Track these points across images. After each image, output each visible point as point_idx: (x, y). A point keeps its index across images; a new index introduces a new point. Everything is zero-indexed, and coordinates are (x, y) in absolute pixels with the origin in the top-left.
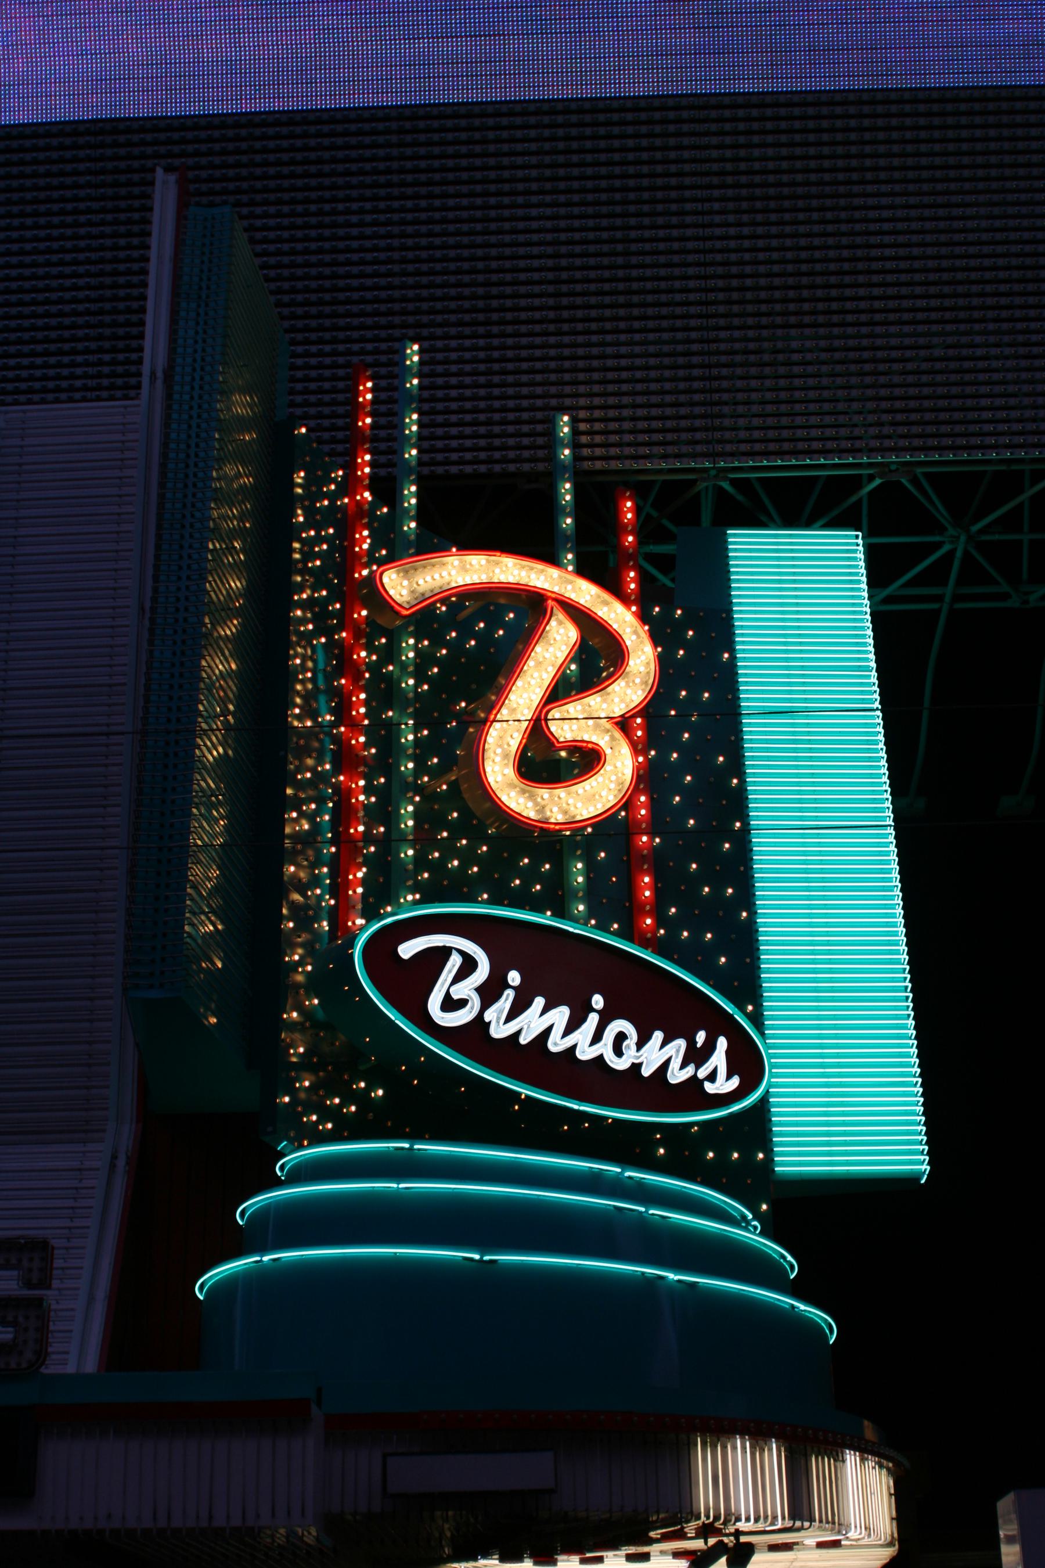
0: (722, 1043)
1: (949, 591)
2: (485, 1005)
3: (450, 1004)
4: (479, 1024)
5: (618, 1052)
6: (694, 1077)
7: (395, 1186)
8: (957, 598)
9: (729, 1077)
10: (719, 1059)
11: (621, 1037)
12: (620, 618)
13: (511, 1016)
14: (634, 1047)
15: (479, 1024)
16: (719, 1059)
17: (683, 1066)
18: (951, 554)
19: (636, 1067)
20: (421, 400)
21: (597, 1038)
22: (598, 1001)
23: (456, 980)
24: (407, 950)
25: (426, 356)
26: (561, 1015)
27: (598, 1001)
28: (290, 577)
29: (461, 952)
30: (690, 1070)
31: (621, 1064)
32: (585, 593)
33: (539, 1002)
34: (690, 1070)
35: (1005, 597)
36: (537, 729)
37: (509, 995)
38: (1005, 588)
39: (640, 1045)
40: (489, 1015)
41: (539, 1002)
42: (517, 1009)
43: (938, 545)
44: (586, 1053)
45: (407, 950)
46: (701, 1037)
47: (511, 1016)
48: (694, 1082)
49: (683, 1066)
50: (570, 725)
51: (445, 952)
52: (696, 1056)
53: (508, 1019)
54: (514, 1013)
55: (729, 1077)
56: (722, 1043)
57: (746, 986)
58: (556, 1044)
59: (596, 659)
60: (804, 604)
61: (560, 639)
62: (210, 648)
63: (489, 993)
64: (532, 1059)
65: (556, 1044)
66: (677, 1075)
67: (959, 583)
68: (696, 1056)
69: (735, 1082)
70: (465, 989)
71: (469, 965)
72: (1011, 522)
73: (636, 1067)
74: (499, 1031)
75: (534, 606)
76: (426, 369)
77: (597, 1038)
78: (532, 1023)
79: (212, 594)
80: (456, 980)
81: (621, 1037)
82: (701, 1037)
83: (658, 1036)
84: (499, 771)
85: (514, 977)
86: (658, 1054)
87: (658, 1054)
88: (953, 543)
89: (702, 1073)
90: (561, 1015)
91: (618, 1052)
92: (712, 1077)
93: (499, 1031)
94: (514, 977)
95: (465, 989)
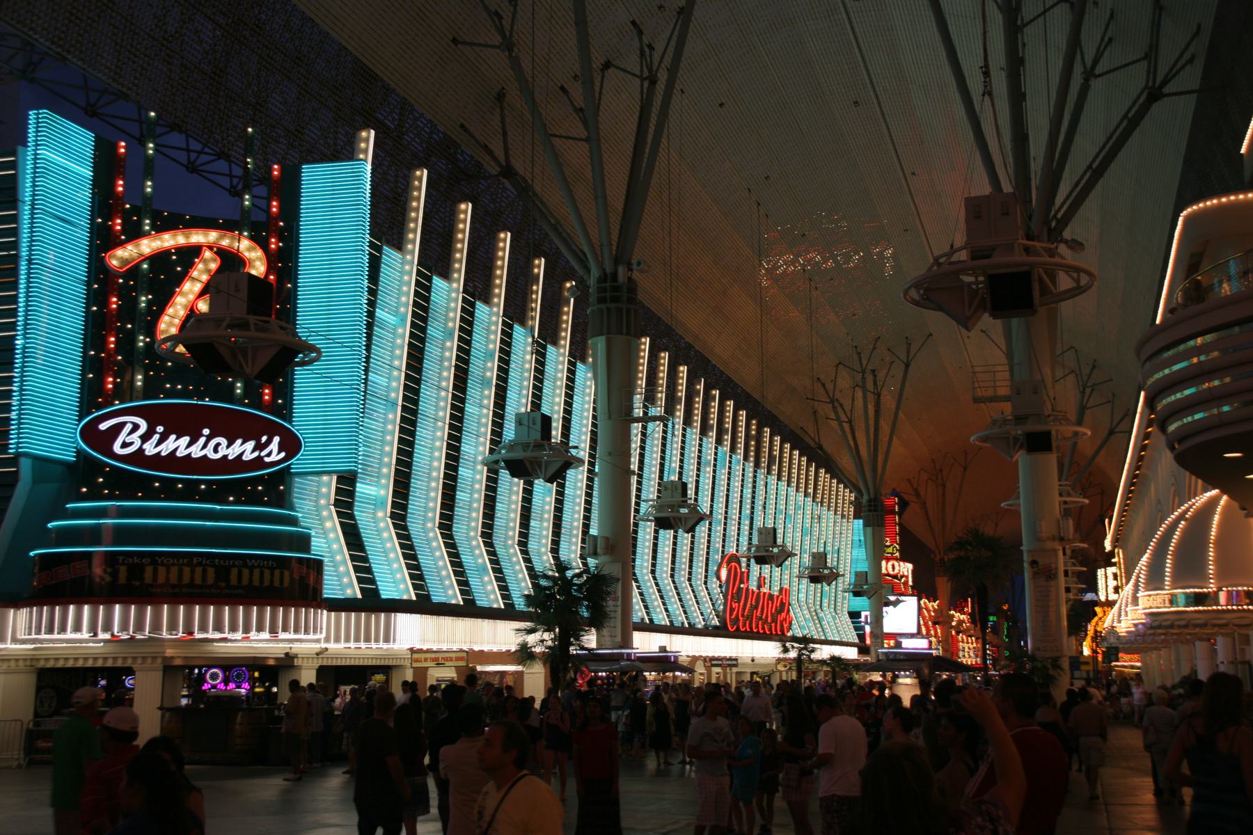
4: (141, 450)
7: (1185, 421)
9: (279, 452)
10: (274, 445)
11: (218, 444)
15: (141, 450)
16: (274, 445)
20: (1024, 683)
23: (130, 434)
24: (103, 426)
26: (185, 440)
30: (256, 454)
34: (256, 454)
37: (157, 437)
40: (145, 446)
45: (103, 426)
48: (260, 458)
51: (124, 424)
54: (159, 443)
55: (279, 452)
56: (277, 439)
63: (145, 438)
64: (170, 462)
66: (248, 457)
68: (259, 447)
69: (283, 455)
70: (135, 437)
71: (136, 427)
73: (225, 457)
79: (634, 479)
81: (218, 444)
82: (264, 439)
86: (244, 449)
87: (244, 449)
89: (263, 454)
90: (250, 445)
92: (269, 455)
95: (135, 437)
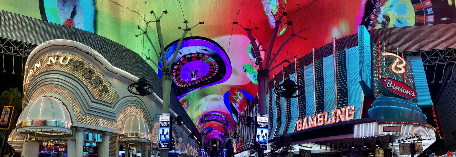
3: (389, 85)
10: (413, 93)
12: (402, 59)
16: (413, 93)
24: (385, 80)
26: (399, 88)
28: (450, 6)
32: (400, 57)
36: (396, 66)
45: (385, 80)
50: (399, 66)
52: (411, 93)
58: (399, 90)
62: (295, 101)
63: (393, 85)
65: (399, 90)
68: (411, 93)
72: (432, 56)
75: (396, 58)
78: (396, 88)
84: (387, 85)
88: (428, 58)
90: (399, 88)
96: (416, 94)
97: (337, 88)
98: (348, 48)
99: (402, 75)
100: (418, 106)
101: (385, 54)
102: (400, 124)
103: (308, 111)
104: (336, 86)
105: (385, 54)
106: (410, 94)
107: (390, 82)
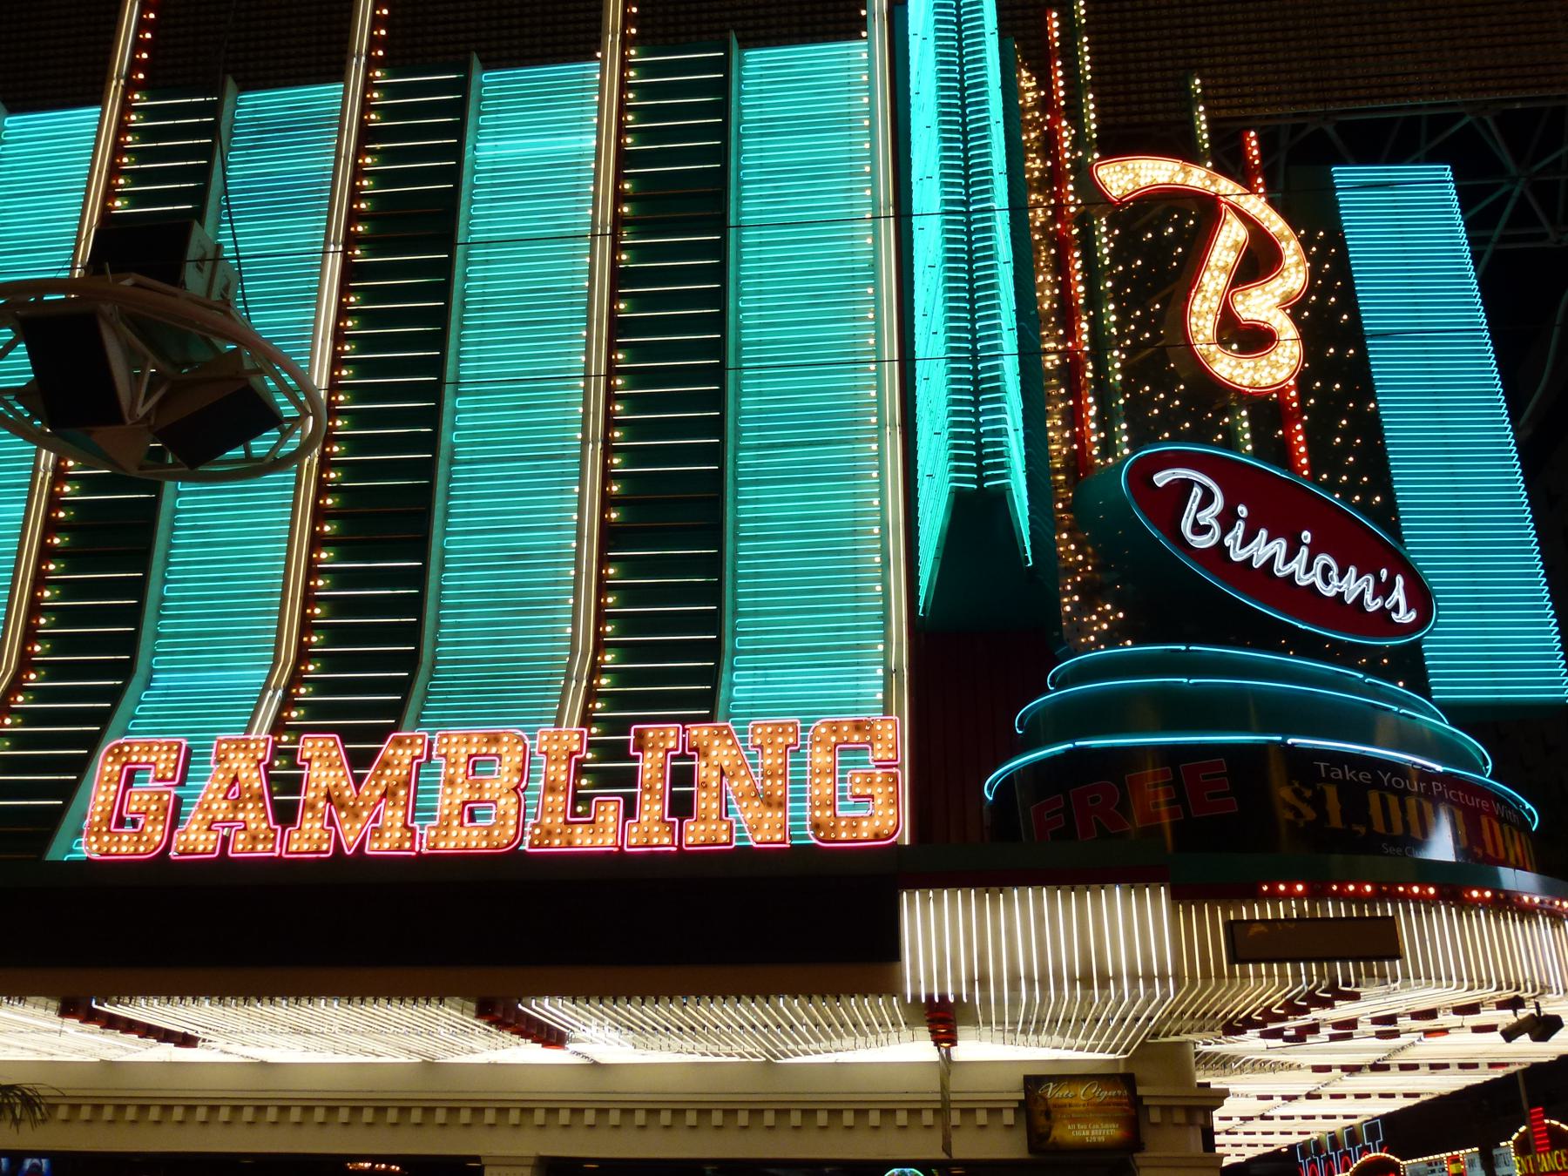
0: (1399, 580)
1: (1496, 234)
2: (1224, 533)
3: (1200, 529)
5: (1327, 582)
6: (1383, 607)
8: (1503, 239)
10: (1399, 594)
13: (1245, 544)
14: (1336, 578)
15: (1221, 549)
16: (1399, 594)
17: (1374, 598)
18: (1508, 195)
19: (1340, 595)
21: (1309, 569)
22: (1306, 536)
24: (1162, 479)
25: (1092, 18)
27: (1306, 536)
29: (1201, 485)
30: (1379, 601)
31: (1329, 592)
33: (1263, 533)
35: (1544, 236)
38: (1548, 228)
39: (1341, 576)
40: (1228, 541)
41: (1263, 533)
42: (1248, 539)
43: (1497, 187)
44: (1303, 580)
45: (1162, 479)
46: (1384, 573)
47: (1245, 544)
49: (1374, 598)
51: (1187, 485)
52: (1384, 590)
53: (1243, 546)
56: (1399, 580)
57: (1388, 515)
58: (1280, 569)
59: (1258, 261)
60: (1412, 228)
61: (1197, 492)
63: (1227, 520)
64: (1261, 579)
65: (1280, 569)
66: (1372, 605)
67: (1508, 225)
69: (1413, 615)
71: (1207, 499)
73: (1340, 595)
74: (1238, 555)
76: (1092, 28)
77: (1309, 569)
80: (1200, 509)
82: (1384, 573)
83: (1353, 570)
85: (1243, 510)
86: (1352, 586)
87: (1352, 586)
91: (1327, 582)
93: (1238, 555)
94: (1243, 510)
95: (1208, 517)
96: (1420, 596)
97: (608, 477)
98: (489, 65)
99: (1267, 409)
100: (1456, 712)
101: (1125, 177)
102: (1395, 898)
103: (461, 624)
104: (595, 451)
105: (1125, 177)
106: (1372, 605)
107: (1207, 499)
